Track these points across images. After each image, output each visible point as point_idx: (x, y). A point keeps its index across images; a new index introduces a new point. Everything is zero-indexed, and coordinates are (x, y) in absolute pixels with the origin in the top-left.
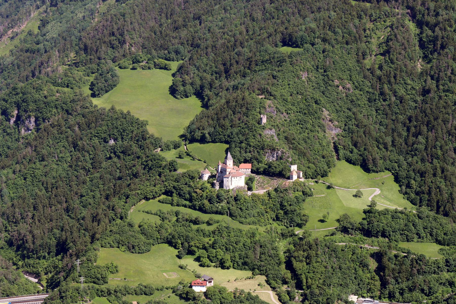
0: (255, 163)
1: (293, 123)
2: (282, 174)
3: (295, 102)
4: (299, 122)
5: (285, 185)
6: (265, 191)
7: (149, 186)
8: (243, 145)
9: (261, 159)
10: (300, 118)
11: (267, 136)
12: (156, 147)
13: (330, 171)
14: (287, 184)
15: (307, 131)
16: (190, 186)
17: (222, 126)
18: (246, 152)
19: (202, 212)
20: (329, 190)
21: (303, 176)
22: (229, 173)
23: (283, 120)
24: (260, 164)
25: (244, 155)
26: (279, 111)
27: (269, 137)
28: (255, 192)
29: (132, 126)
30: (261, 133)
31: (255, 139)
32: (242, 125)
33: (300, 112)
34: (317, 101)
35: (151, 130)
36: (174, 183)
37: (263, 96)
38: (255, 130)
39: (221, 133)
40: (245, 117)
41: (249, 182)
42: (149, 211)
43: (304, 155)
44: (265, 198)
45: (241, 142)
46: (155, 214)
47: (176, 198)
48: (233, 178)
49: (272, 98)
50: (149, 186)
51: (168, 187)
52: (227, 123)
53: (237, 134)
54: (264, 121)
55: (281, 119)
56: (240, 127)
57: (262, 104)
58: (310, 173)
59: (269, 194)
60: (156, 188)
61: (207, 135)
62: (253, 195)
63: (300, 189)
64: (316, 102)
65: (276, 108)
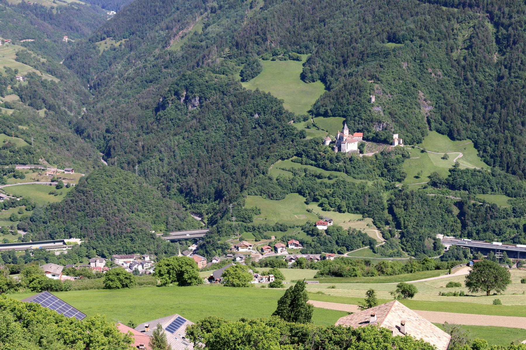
0: (366, 132)
6: (373, 154)
8: (357, 118)
10: (401, 98)
14: (390, 148)
16: (315, 150)
17: (341, 104)
18: (359, 124)
25: (357, 126)
28: (366, 154)
30: (370, 109)
32: (356, 103)
35: (286, 107)
37: (372, 81)
41: (361, 148)
43: (404, 126)
45: (355, 116)
47: (304, 159)
49: (379, 82)
51: (299, 150)
52: (344, 101)
53: (352, 110)
54: (373, 100)
55: (386, 98)
59: (376, 156)
63: (400, 152)
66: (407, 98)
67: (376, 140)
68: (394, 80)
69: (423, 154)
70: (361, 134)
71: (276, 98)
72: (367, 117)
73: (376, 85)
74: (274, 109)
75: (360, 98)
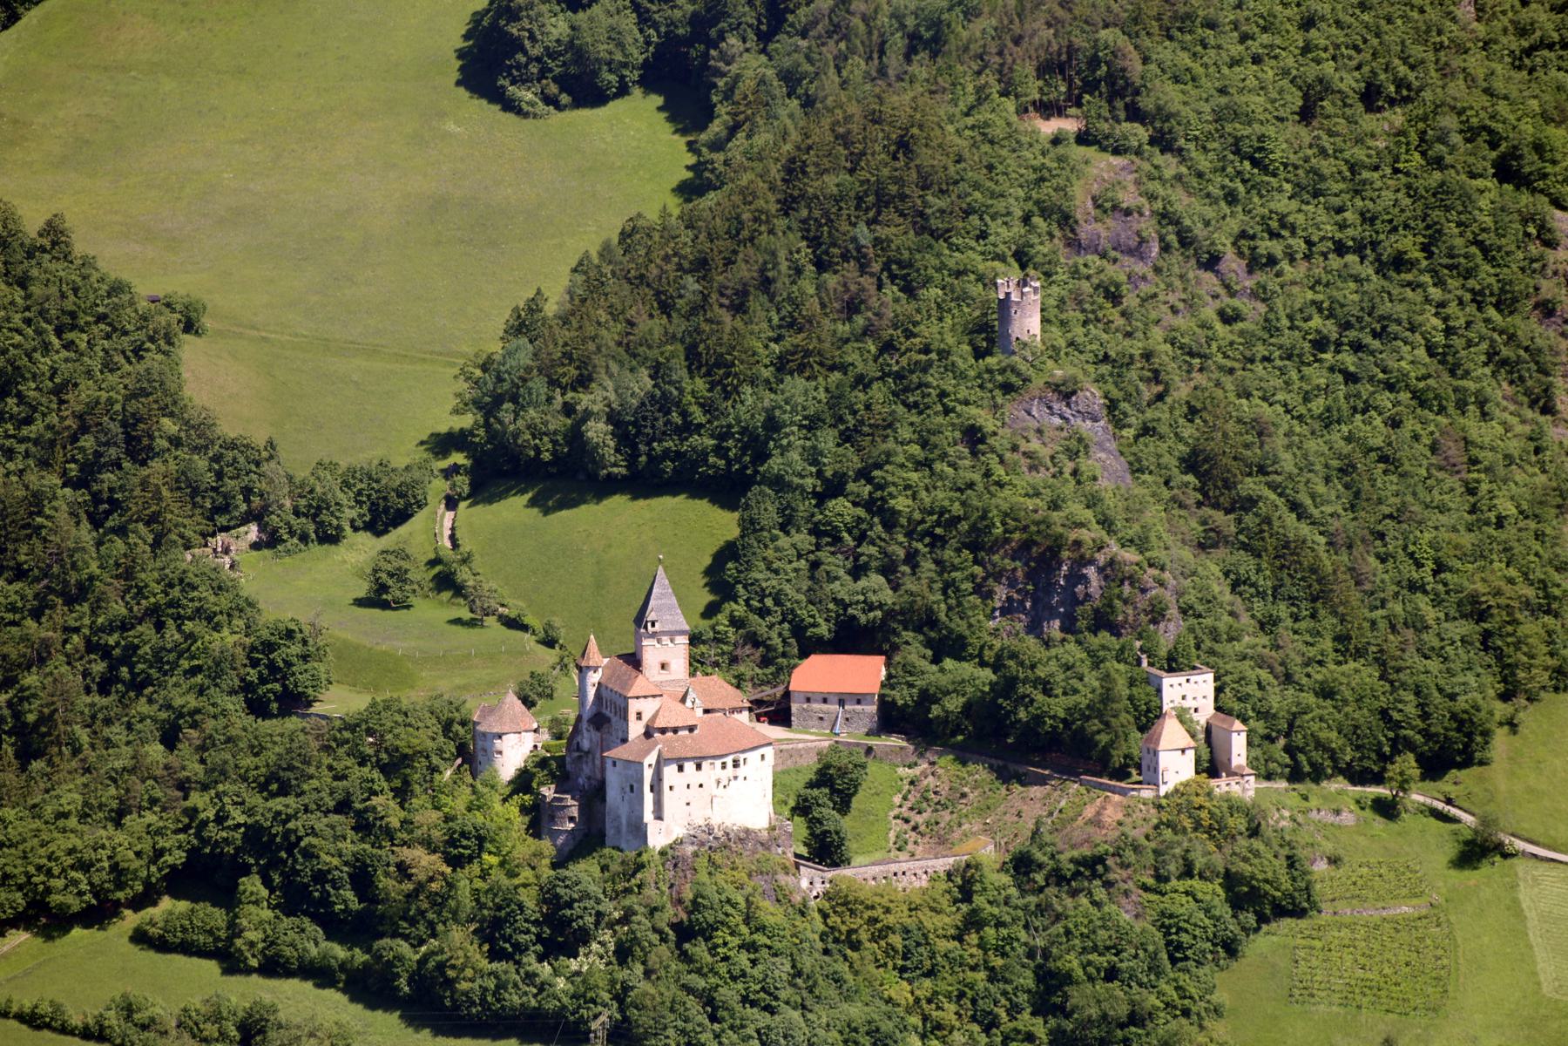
0: (914, 650)
1: (1288, 338)
2: (1089, 749)
3: (1327, 166)
4: (1330, 329)
5: (1096, 822)
6: (943, 864)
7: (73, 822)
8: (841, 509)
9: (960, 626)
10: (1349, 294)
11: (1035, 445)
12: (222, 520)
13: (1512, 725)
14: (1112, 815)
15: (1384, 399)
16: (365, 826)
17: (717, 368)
18: (857, 572)
19: (439, 1031)
20: (1467, 873)
21: (1252, 762)
22: (648, 734)
23: (1209, 312)
24: (948, 663)
25: (844, 588)
26: (1185, 240)
27: (1044, 452)
28: (863, 872)
29: (69, 345)
30: (983, 418)
31: (926, 464)
32: (861, 357)
33: (1359, 249)
34: (1514, 154)
35: (213, 383)
36: (255, 800)
37: (1070, 126)
38: (943, 394)
39: (699, 416)
40: (891, 291)
41: (823, 806)
42: (45, 1008)
43: (1320, 595)
44: (930, 921)
45: (833, 487)
46: (86, 1034)
47: (258, 914)
48: (670, 772)
49: (1139, 133)
50: (73, 822)
51: (213, 831)
52: (758, 336)
53: (812, 424)
54: (1028, 324)
55: (1177, 308)
56: (843, 368)
57: (1047, 189)
58: (1333, 738)
59: (965, 883)
60: (120, 837)
61: (597, 431)
62: (840, 901)
63: (1204, 852)
64: (1507, 171)
65: (1165, 217)
66: (1422, 305)
67: (1011, 737)
68: (1306, 114)
69: (1489, 872)
70: (864, 673)
71: (117, 289)
72: (941, 496)
73: (1102, 165)
74: (86, 391)
75: (906, 307)
